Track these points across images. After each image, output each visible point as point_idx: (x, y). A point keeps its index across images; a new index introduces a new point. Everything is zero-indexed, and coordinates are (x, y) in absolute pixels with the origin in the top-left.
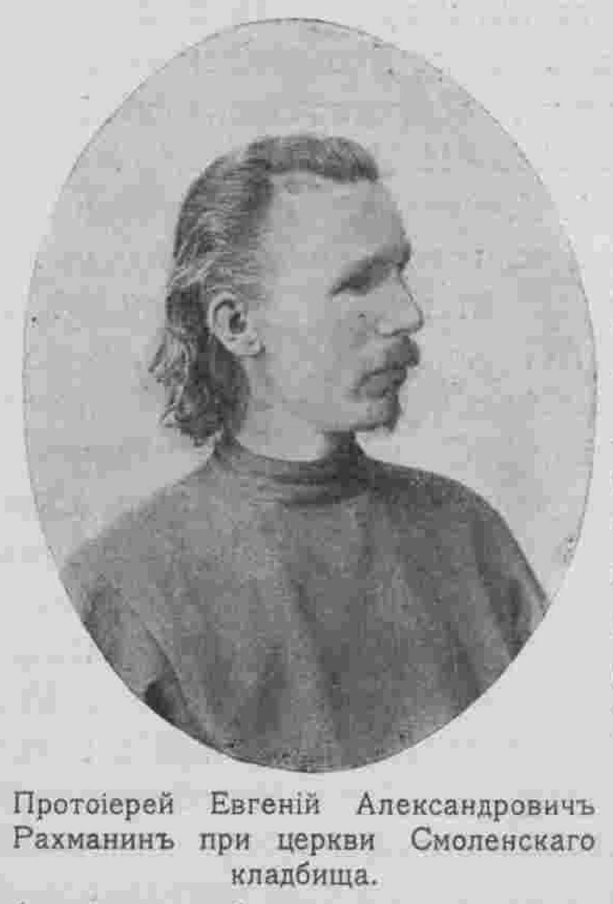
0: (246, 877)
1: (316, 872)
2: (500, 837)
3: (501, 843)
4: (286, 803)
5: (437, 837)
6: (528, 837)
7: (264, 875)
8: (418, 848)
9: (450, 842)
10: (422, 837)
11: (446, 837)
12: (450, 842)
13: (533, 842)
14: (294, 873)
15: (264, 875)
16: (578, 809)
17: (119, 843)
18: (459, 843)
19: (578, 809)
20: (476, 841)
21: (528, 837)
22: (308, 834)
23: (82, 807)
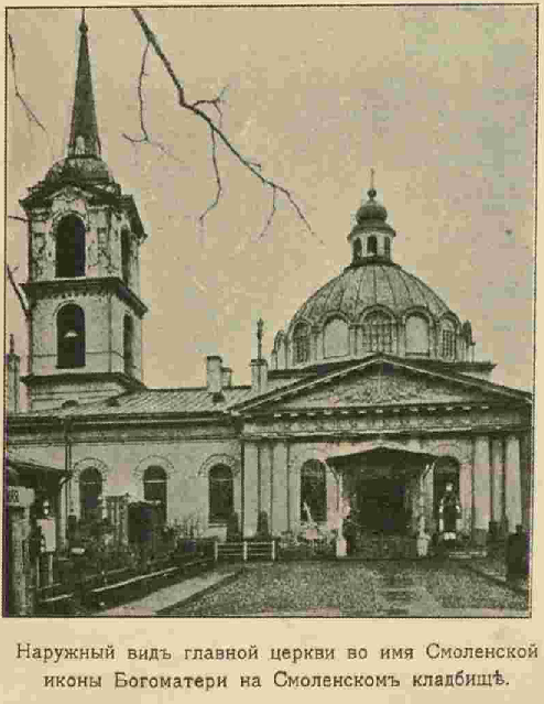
0: (422, 681)
1: (468, 676)
2: (484, 649)
3: (332, 682)
4: (338, 684)
5: (290, 678)
6: (503, 649)
7: (434, 680)
8: (428, 653)
9: (236, 654)
10: (281, 679)
11: (297, 678)
12: (236, 654)
13: (353, 681)
14: (454, 677)
15: (434, 680)
16: (389, 682)
17: (55, 680)
18: (458, 653)
19: (389, 682)
20: (469, 652)
21: (503, 649)
22: (204, 677)
23: (146, 683)
